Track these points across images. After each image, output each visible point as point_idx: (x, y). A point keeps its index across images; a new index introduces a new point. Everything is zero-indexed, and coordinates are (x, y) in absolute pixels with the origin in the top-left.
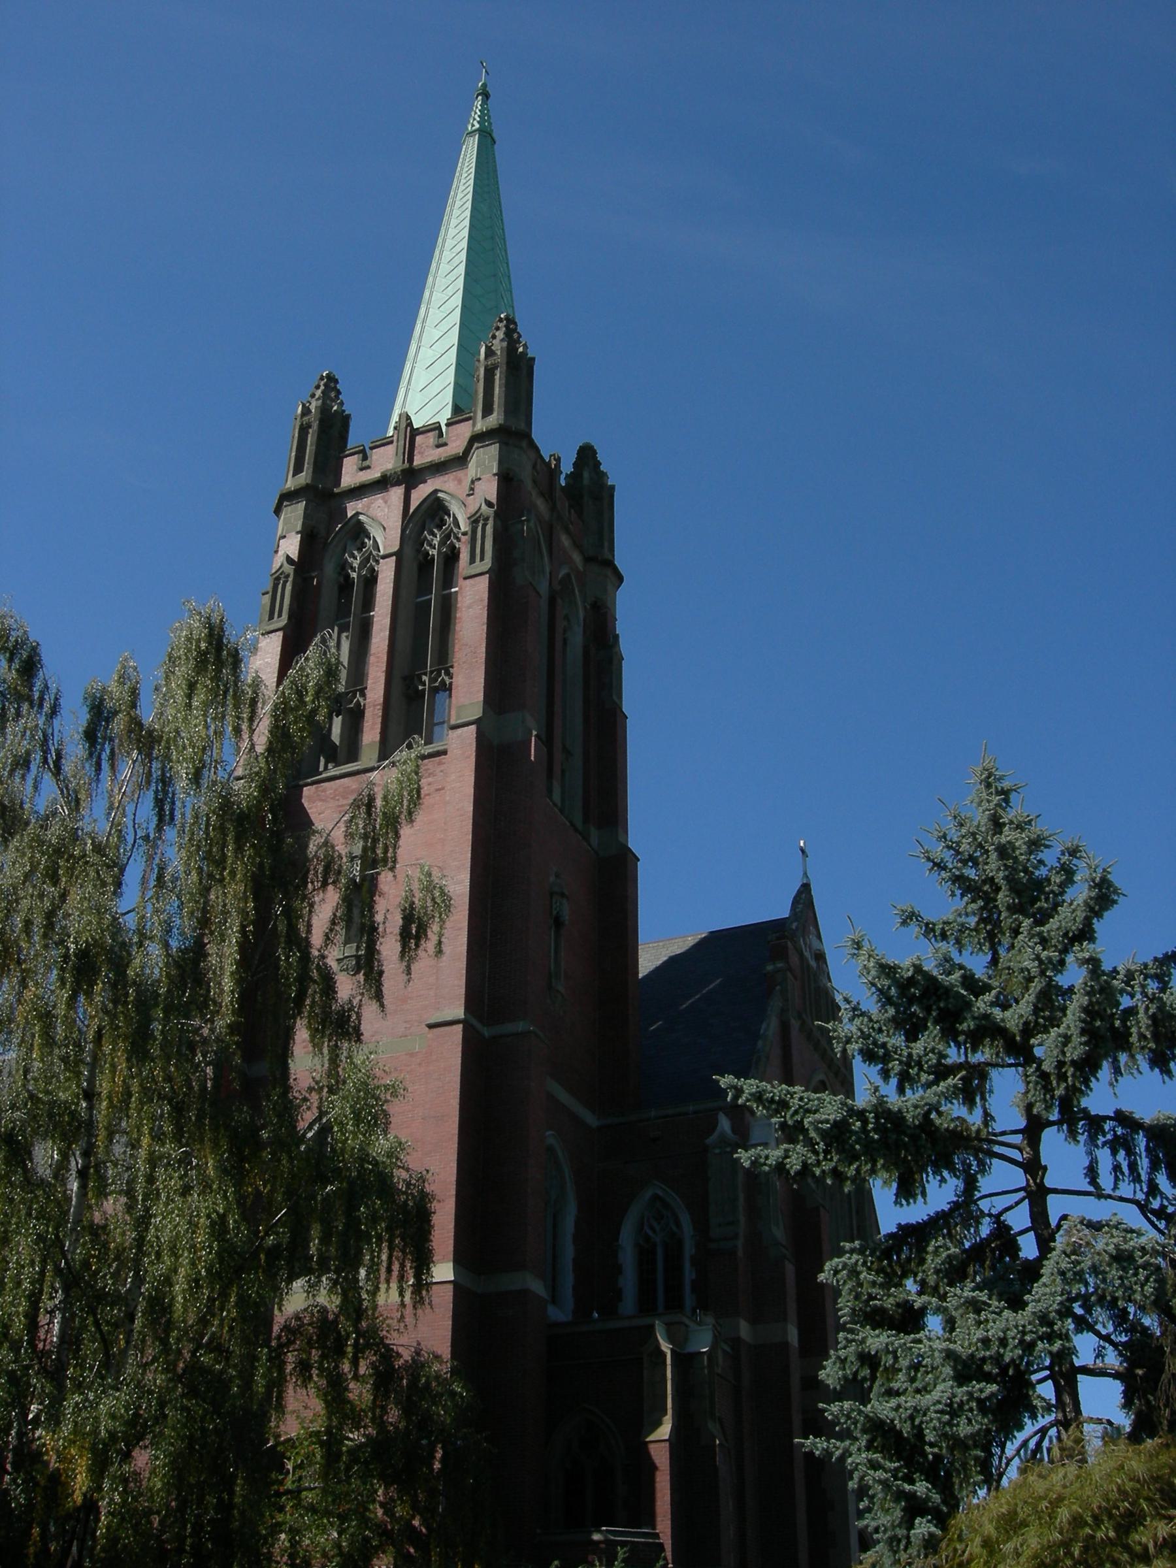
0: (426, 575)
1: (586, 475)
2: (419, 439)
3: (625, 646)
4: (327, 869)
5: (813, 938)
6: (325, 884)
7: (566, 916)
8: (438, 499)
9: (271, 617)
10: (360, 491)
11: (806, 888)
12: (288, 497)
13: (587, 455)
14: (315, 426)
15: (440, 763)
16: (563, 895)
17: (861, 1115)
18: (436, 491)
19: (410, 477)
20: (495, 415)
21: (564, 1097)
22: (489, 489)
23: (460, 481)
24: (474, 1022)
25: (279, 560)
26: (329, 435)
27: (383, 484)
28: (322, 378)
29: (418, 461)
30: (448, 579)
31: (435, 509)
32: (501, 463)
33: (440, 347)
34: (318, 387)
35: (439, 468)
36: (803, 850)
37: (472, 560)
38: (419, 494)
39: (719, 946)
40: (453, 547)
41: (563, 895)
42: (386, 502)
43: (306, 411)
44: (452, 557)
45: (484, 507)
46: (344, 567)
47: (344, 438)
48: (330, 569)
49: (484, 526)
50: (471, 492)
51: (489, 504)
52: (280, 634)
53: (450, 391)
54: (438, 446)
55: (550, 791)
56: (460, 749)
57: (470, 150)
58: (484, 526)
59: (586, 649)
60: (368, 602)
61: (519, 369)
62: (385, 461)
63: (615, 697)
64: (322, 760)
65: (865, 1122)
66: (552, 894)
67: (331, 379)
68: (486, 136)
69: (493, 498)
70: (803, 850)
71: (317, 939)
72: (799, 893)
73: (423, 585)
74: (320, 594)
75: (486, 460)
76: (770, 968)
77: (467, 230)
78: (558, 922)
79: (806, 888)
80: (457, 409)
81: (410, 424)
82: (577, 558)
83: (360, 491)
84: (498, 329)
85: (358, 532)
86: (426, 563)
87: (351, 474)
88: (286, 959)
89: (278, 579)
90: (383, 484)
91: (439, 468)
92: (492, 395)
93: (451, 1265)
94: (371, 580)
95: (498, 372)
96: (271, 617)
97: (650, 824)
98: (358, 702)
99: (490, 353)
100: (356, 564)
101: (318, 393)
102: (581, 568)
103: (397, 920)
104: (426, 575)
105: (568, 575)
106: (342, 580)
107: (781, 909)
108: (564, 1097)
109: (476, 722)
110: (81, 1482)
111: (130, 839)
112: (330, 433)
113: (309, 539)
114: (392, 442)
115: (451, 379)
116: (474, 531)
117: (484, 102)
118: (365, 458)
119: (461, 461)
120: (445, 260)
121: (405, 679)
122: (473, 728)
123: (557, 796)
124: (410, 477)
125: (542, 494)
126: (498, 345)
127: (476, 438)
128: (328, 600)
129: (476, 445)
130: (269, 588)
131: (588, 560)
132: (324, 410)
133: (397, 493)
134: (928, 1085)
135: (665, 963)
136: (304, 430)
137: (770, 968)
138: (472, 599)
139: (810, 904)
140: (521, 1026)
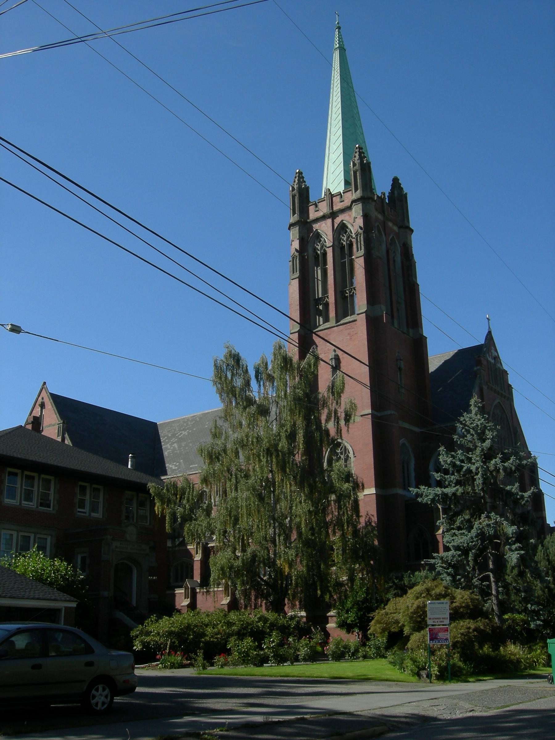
0: (343, 252)
1: (396, 192)
2: (334, 198)
3: (416, 258)
4: (324, 403)
5: (493, 351)
6: (324, 407)
7: (402, 366)
8: (344, 223)
9: (293, 273)
10: (317, 220)
11: (490, 333)
12: (292, 225)
13: (396, 182)
14: (297, 195)
15: (356, 324)
16: (401, 360)
17: (438, 496)
18: (342, 220)
19: (333, 215)
20: (359, 191)
21: (406, 425)
22: (360, 222)
23: (350, 216)
24: (375, 413)
25: (293, 251)
26: (302, 198)
27: (324, 218)
28: (297, 173)
29: (335, 208)
30: (351, 254)
31: (343, 227)
32: (363, 211)
33: (337, 127)
34: (296, 177)
35: (342, 211)
36: (488, 319)
37: (358, 251)
38: (338, 220)
39: (462, 355)
40: (351, 241)
41: (401, 360)
42: (326, 224)
43: (293, 188)
44: (351, 245)
45: (359, 230)
46: (315, 249)
47: (308, 202)
48: (310, 251)
49: (360, 236)
50: (354, 221)
51: (361, 228)
52: (298, 279)
53: (342, 173)
54: (341, 202)
55: (393, 324)
56: (361, 320)
57: (336, 56)
58: (360, 236)
59: (402, 262)
60: (325, 263)
61: (365, 169)
62: (324, 208)
63: (414, 279)
64: (317, 317)
65: (439, 497)
66: (397, 360)
67: (300, 173)
68: (342, 49)
69: (362, 225)
70: (488, 319)
71: (323, 422)
72: (487, 335)
73: (343, 255)
74: (308, 260)
75: (357, 210)
76: (475, 369)
77: (340, 93)
78: (400, 369)
79: (490, 333)
80: (347, 183)
81: (330, 193)
82: (395, 228)
83: (317, 220)
84: (356, 152)
85: (318, 236)
86: (342, 247)
87: (313, 215)
88: (317, 435)
89: (293, 258)
90: (324, 218)
91: (342, 211)
92: (357, 180)
93: (374, 489)
94: (325, 254)
95: (358, 173)
96: (293, 273)
97: (428, 330)
98: (327, 301)
99: (354, 165)
100: (319, 248)
101: (296, 180)
102: (397, 231)
103: (343, 415)
104: (343, 252)
105: (393, 237)
106: (315, 254)
107: (481, 340)
108: (406, 425)
109: (365, 312)
110: (287, 570)
111: (271, 401)
112: (302, 198)
113: (303, 241)
114: (324, 200)
115: (342, 168)
116: (357, 238)
117: (339, 32)
118: (316, 206)
119: (349, 208)
120: (334, 95)
121: (341, 292)
122: (364, 314)
123: (396, 325)
124: (333, 215)
125: (380, 213)
126: (357, 162)
127: (353, 201)
128: (311, 260)
129: (354, 204)
130: (291, 259)
131: (400, 227)
132: (300, 188)
133: (329, 221)
134: (454, 487)
135: (443, 363)
136: (294, 197)
137: (475, 369)
138: (359, 264)
139: (492, 339)
140: (389, 412)
